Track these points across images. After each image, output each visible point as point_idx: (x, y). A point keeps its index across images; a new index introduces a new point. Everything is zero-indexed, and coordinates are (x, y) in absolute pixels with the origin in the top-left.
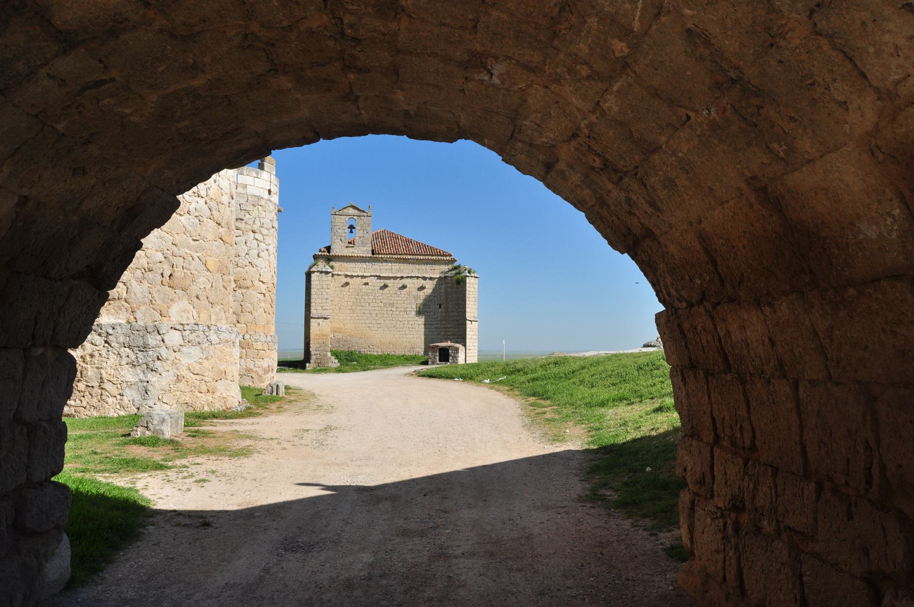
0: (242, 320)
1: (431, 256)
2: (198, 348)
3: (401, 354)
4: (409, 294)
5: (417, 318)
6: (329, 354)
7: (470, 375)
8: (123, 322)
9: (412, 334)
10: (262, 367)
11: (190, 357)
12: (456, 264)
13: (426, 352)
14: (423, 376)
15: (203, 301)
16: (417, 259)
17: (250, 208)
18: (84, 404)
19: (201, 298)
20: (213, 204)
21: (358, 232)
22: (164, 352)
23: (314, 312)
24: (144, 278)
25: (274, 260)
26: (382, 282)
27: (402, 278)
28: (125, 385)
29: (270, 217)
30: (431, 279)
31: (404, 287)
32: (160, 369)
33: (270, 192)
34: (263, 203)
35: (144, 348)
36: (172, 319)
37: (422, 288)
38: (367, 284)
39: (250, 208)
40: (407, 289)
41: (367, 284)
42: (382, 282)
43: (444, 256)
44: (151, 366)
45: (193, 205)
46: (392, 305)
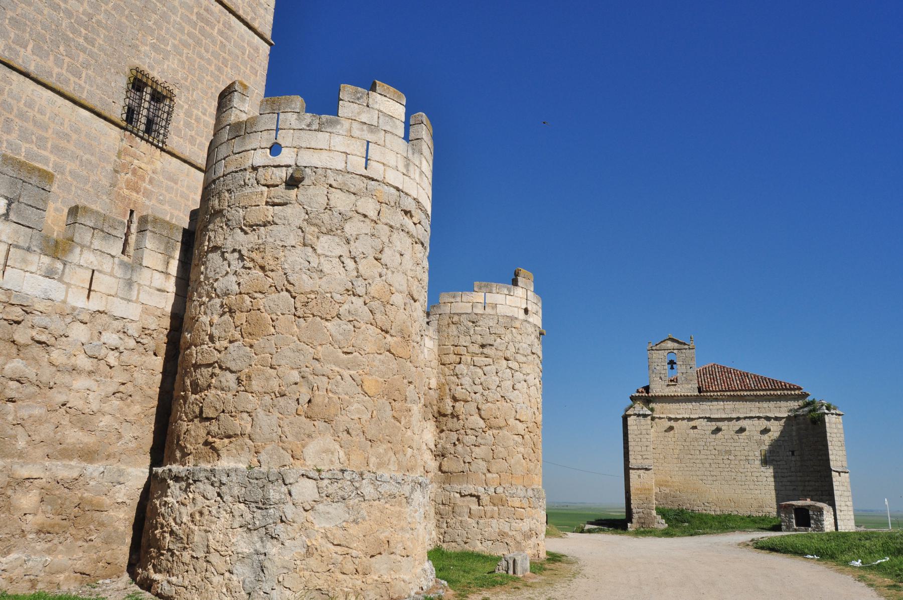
0: (493, 469)
1: (774, 391)
2: (341, 505)
3: (746, 515)
4: (749, 438)
5: (763, 469)
6: (654, 512)
7: (834, 551)
8: (243, 466)
9: (760, 490)
10: (520, 531)
11: (329, 519)
12: (809, 399)
13: (778, 513)
14: (762, 548)
15: (358, 439)
16: (756, 396)
17: (502, 331)
18: (186, 583)
19: (353, 433)
20: (375, 304)
21: (680, 368)
22: (289, 511)
23: (633, 462)
24: (274, 406)
25: (536, 394)
26: (713, 425)
27: (738, 419)
28: (235, 557)
29: (530, 342)
30: (776, 419)
31: (742, 430)
32: (283, 536)
33: (526, 311)
34: (517, 324)
35: (264, 504)
36: (308, 463)
37: (766, 431)
38: (695, 428)
39: (502, 331)
40: (746, 433)
41: (695, 428)
42: (713, 425)
43: (791, 389)
44: (271, 530)
45: (346, 306)
46: (729, 452)
